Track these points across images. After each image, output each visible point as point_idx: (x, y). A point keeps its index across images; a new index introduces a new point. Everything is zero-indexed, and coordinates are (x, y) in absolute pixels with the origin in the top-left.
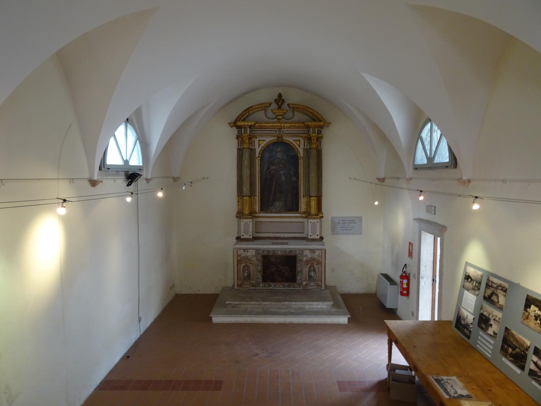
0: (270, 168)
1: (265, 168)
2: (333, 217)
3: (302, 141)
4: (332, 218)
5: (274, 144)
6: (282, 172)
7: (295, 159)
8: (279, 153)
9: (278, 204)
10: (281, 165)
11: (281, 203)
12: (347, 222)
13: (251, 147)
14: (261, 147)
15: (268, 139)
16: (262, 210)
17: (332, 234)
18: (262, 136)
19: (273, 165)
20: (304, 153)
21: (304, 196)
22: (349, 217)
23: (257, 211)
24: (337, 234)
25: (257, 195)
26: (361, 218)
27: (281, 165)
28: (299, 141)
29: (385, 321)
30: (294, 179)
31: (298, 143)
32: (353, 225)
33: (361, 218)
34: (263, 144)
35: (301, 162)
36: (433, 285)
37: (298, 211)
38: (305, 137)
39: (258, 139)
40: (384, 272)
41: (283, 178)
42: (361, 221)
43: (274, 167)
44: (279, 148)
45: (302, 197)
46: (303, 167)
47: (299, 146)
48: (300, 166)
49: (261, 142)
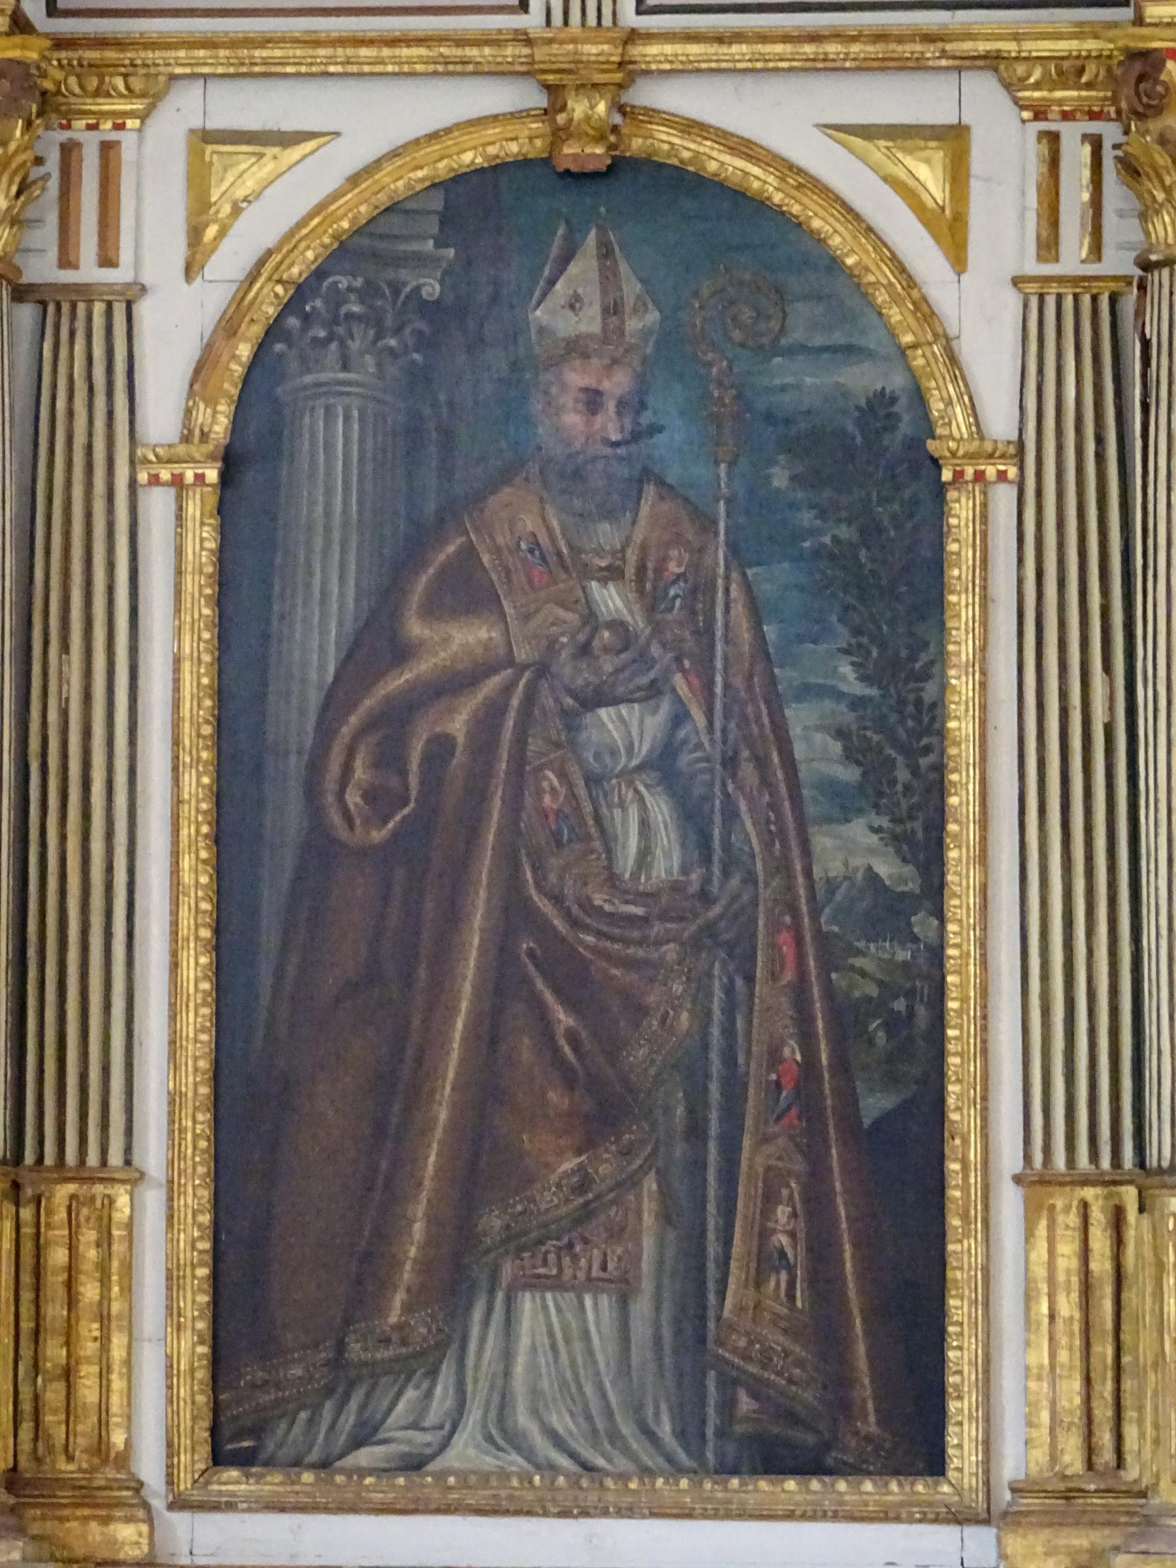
0: (402, 653)
1: (315, 643)
3: (1003, 141)
5: (488, 211)
6: (625, 729)
7: (872, 491)
8: (576, 377)
9: (551, 1338)
10: (611, 600)
11: (599, 1310)
13: (42, 269)
14: (230, 260)
15: (372, 129)
16: (235, 1439)
18: (249, 65)
19: (466, 592)
20: (1033, 377)
21: (1036, 1182)
23: (150, 1467)
25: (153, 1153)
27: (611, 600)
28: (953, 138)
29: (866, 1126)
30: (852, 849)
31: (928, 173)
34: (281, 205)
35: (986, 547)
36: (486, 118)
37: (935, 1463)
38: (1069, 71)
39: (184, 110)
40: (339, 140)
41: (648, 838)
43: (469, 637)
44: (583, 270)
45: (1010, 1203)
46: (1031, 621)
47: (951, 231)
48: (962, 605)
49: (241, 174)
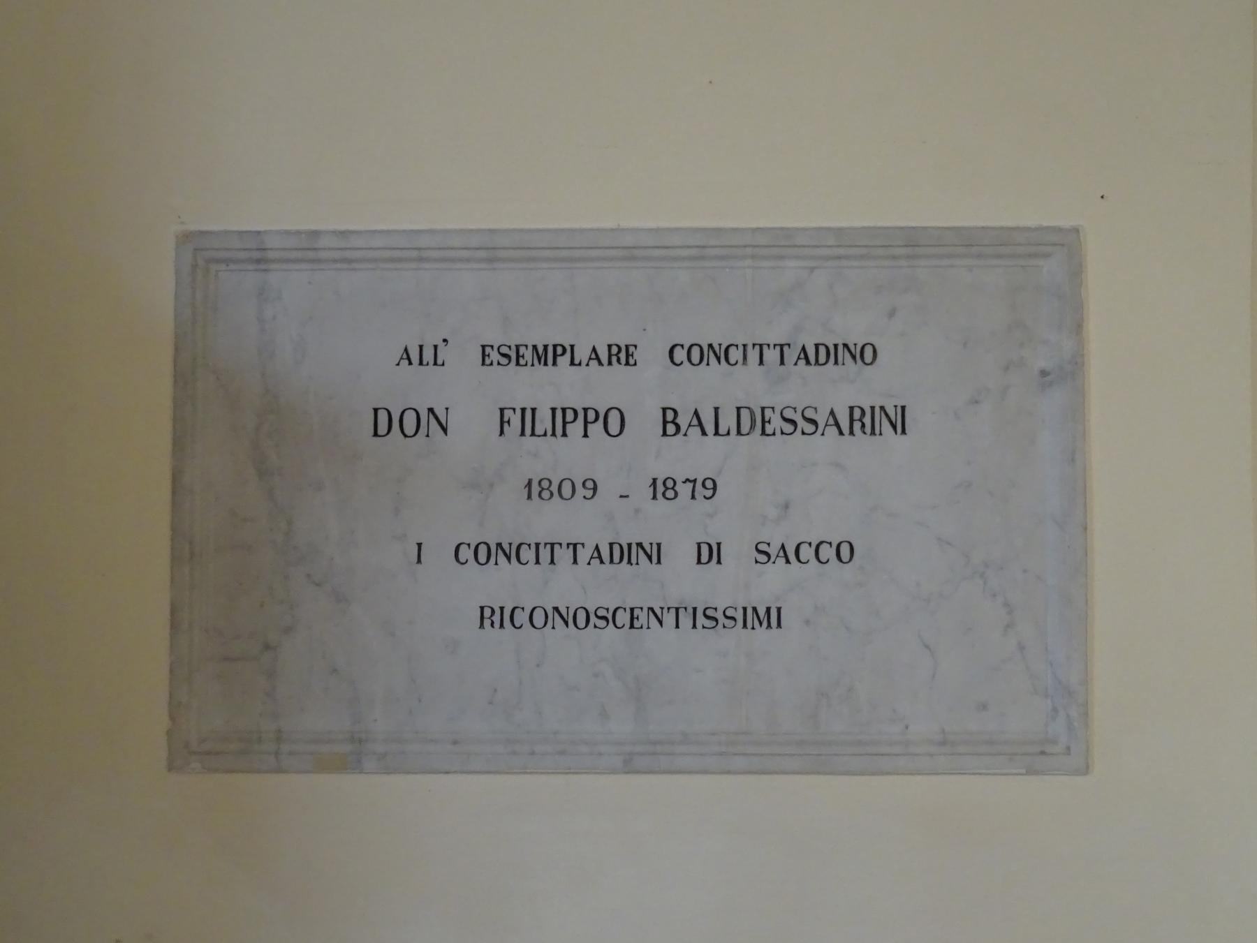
2: (257, 253)
4: (203, 257)
12: (642, 390)
17: (186, 753)
22: (713, 251)
24: (351, 754)
26: (1036, 271)
32: (817, 483)
33: (1036, 271)
42: (1067, 375)
